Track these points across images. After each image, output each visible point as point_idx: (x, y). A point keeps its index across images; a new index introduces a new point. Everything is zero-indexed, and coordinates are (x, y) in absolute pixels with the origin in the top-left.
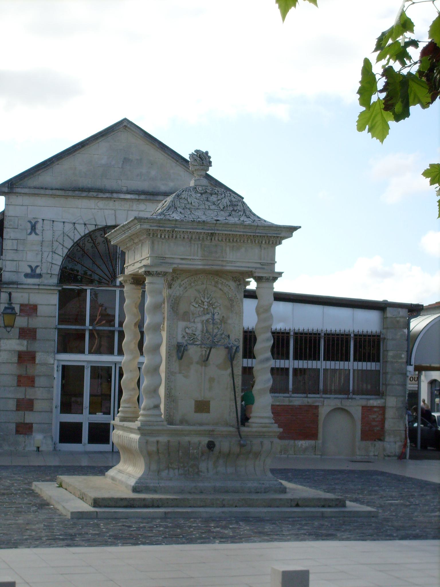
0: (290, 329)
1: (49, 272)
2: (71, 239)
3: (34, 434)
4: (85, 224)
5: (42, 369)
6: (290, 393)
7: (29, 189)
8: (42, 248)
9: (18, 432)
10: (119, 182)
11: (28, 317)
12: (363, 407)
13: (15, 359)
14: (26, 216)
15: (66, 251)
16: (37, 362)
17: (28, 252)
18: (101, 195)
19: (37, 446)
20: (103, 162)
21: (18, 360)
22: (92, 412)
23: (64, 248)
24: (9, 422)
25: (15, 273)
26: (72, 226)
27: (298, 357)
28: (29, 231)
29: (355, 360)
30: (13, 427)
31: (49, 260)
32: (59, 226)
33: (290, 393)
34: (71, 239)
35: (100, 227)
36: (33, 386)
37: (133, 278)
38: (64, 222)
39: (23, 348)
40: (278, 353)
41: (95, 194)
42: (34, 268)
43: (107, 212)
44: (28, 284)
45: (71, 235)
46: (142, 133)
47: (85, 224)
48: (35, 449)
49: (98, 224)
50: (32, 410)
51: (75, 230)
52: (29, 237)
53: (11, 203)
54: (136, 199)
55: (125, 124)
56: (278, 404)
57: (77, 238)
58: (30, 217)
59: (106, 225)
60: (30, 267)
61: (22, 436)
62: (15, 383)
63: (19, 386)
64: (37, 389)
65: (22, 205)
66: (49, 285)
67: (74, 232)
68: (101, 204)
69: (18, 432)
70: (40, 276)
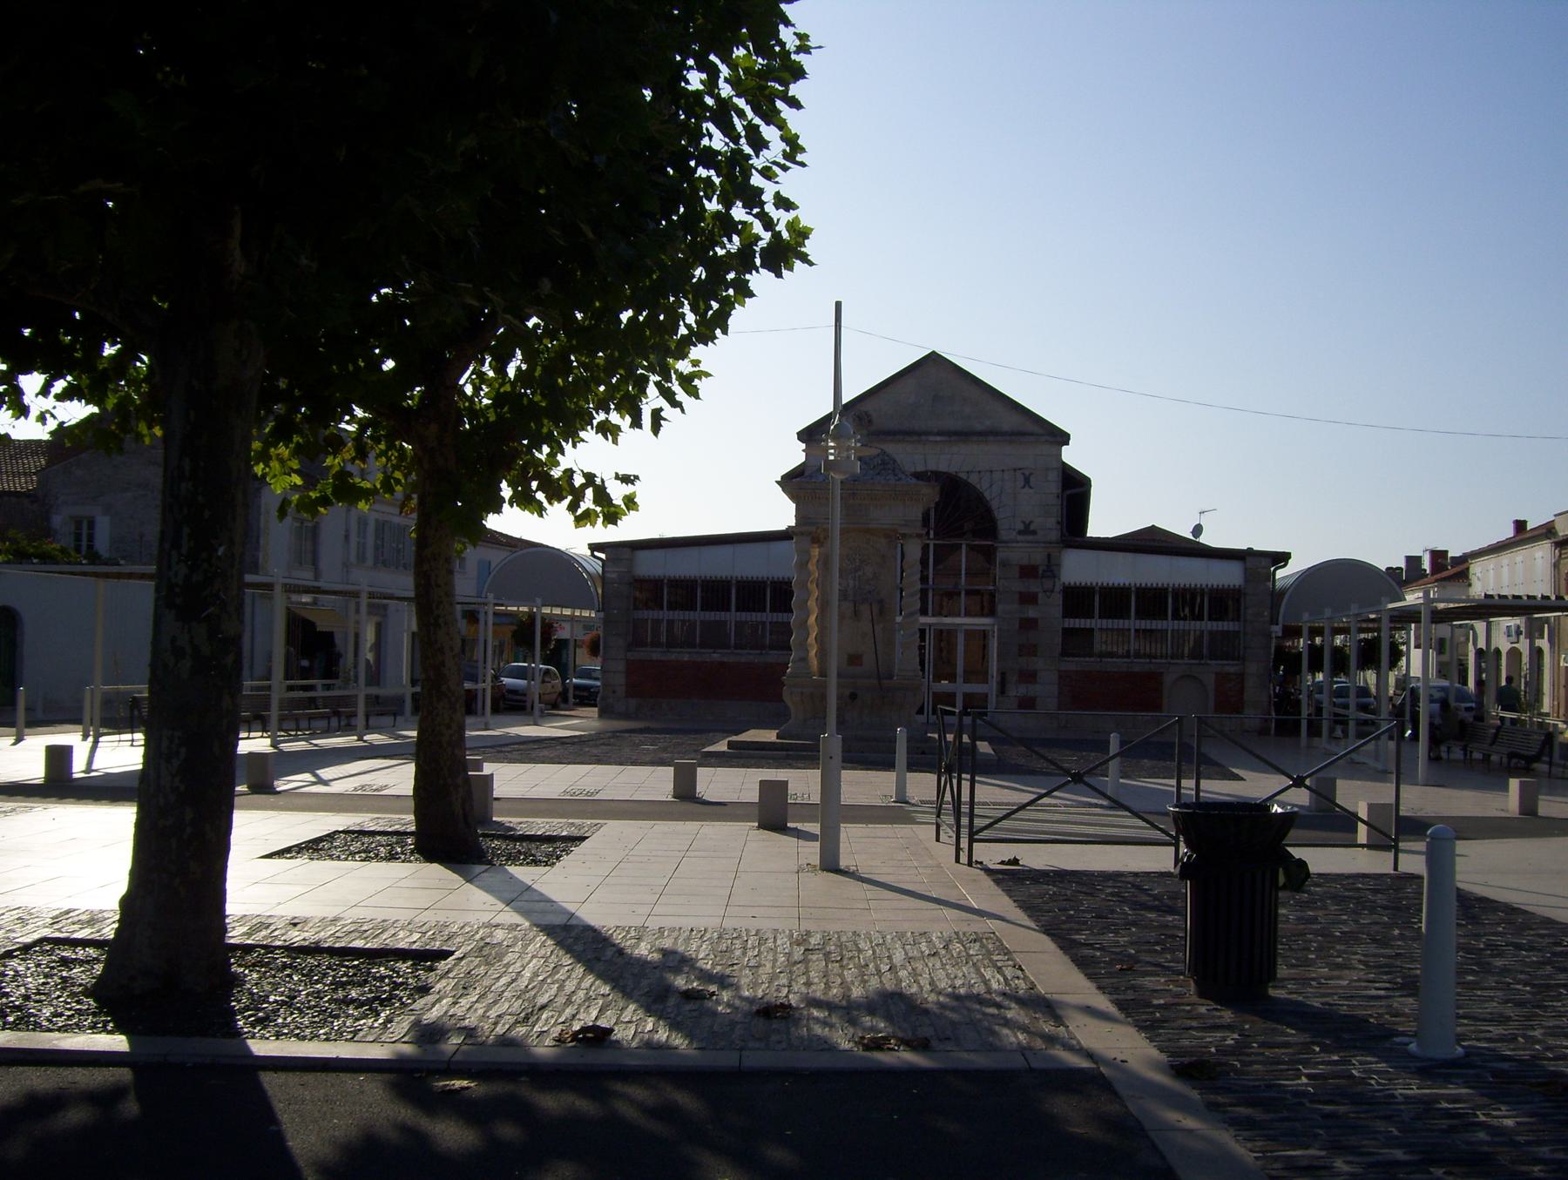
0: (1168, 585)
12: (1216, 673)
29: (737, 610)
41: (901, 437)
56: (1115, 670)
60: (1024, 522)
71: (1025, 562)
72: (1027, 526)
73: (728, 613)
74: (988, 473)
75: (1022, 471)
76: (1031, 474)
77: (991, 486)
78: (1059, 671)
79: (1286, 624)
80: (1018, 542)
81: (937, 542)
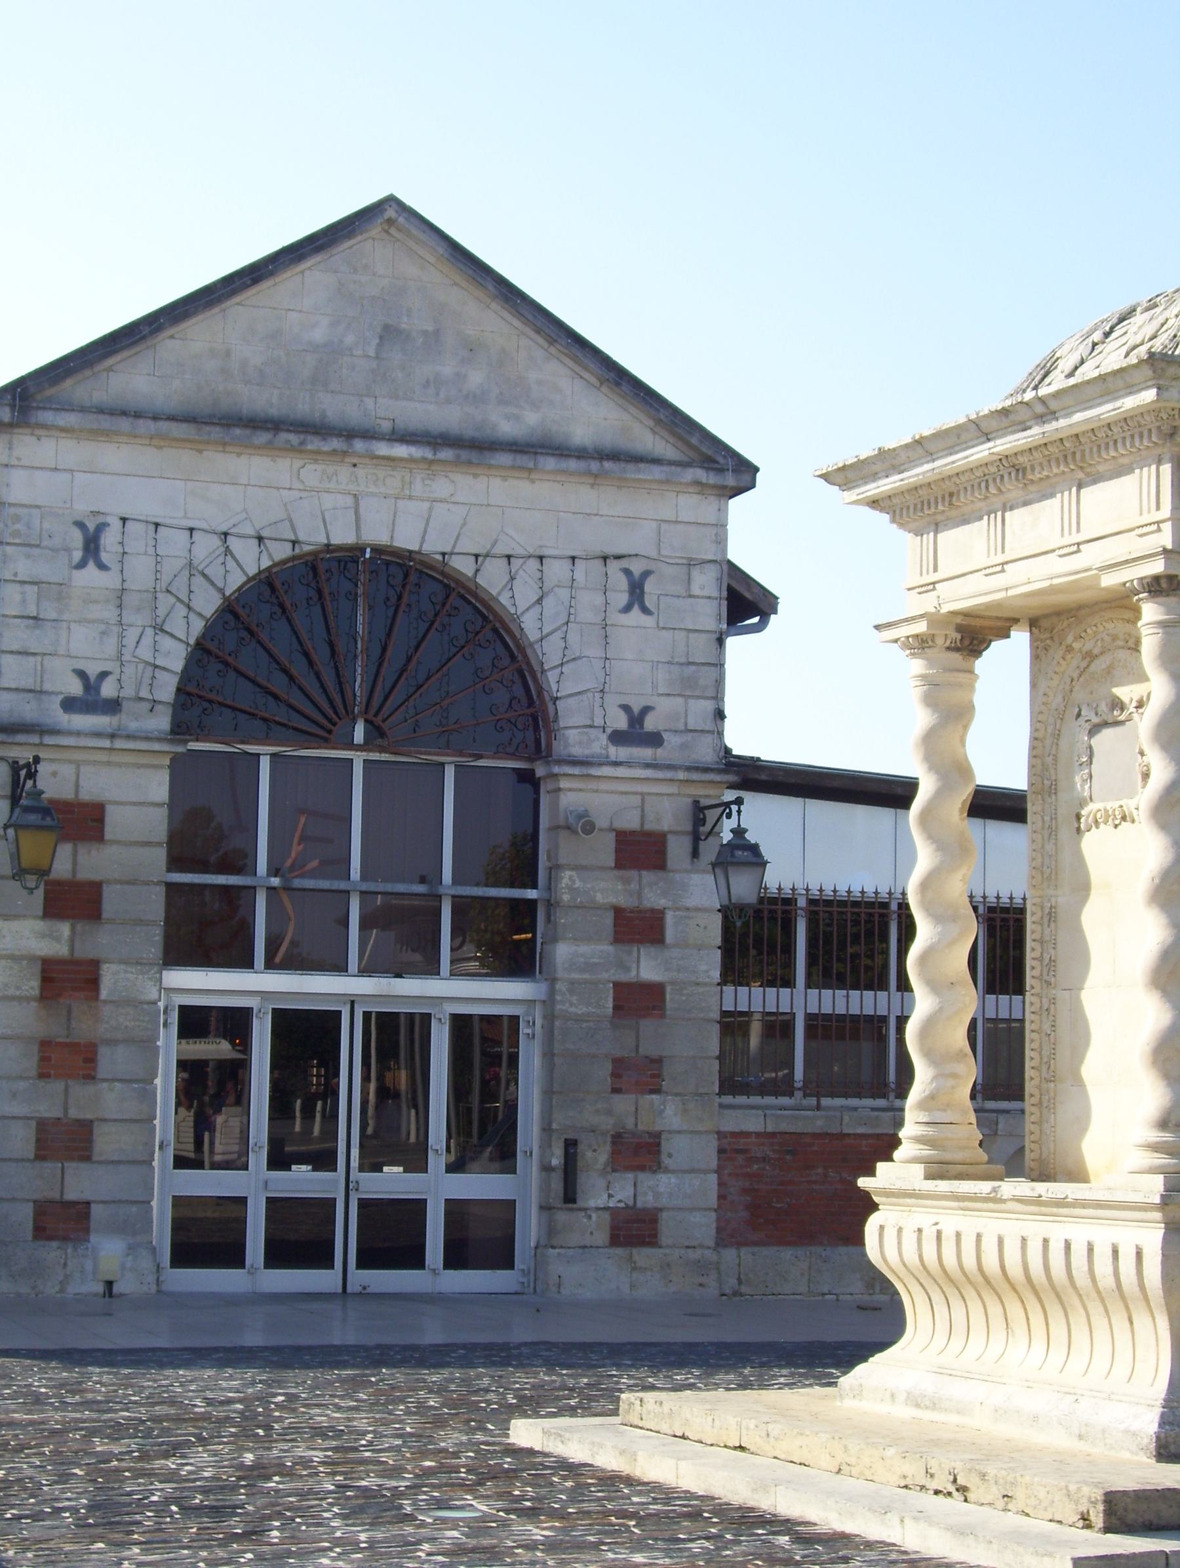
1: (144, 693)
2: (212, 583)
3: (94, 1238)
4: (260, 539)
5: (121, 1019)
6: (799, 1094)
7: (80, 415)
8: (120, 615)
9: (41, 1232)
10: (370, 402)
11: (75, 845)
13: (32, 986)
14: (68, 505)
15: (198, 626)
16: (104, 994)
17: (73, 626)
18: (314, 443)
19: (105, 1279)
20: (319, 335)
21: (42, 989)
22: (279, 1160)
23: (192, 616)
24: (13, 1199)
25: (31, 695)
26: (216, 541)
27: (822, 976)
28: (78, 555)
30: (26, 1213)
31: (145, 653)
32: (174, 544)
33: (799, 1094)
34: (212, 583)
35: (307, 548)
36: (90, 1077)
37: (959, 628)
38: (191, 530)
39: (60, 950)
40: (827, 972)
41: (294, 439)
42: (92, 679)
43: (328, 501)
44: (78, 734)
45: (215, 572)
46: (441, 251)
47: (260, 539)
48: (100, 1288)
49: (301, 539)
50: (87, 1158)
51: (229, 557)
52: (77, 574)
53: (19, 459)
54: (424, 459)
55: (391, 213)
56: (861, 1130)
57: (235, 581)
58: (82, 508)
59: (325, 541)
60: (82, 674)
61: (55, 1244)
62: (31, 1064)
63: (43, 1076)
64: (105, 1085)
65: (56, 469)
66: (147, 739)
67: (224, 563)
68: (312, 473)
69: (41, 1232)
70: (113, 706)
71: (630, 822)
72: (637, 719)
73: (1017, 999)
74: (533, 564)
75: (624, 563)
76: (647, 574)
77: (539, 601)
78: (720, 1135)
79: (668, 989)
80: (616, 764)
81: (375, 756)
